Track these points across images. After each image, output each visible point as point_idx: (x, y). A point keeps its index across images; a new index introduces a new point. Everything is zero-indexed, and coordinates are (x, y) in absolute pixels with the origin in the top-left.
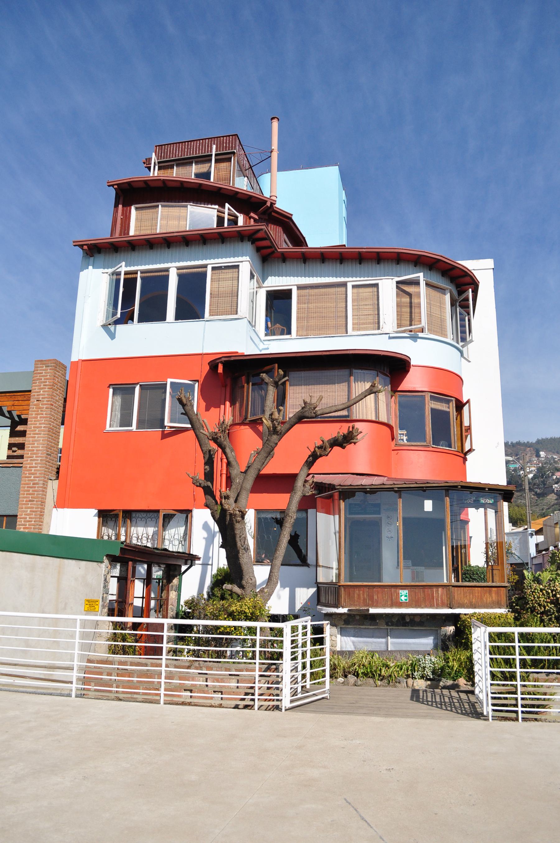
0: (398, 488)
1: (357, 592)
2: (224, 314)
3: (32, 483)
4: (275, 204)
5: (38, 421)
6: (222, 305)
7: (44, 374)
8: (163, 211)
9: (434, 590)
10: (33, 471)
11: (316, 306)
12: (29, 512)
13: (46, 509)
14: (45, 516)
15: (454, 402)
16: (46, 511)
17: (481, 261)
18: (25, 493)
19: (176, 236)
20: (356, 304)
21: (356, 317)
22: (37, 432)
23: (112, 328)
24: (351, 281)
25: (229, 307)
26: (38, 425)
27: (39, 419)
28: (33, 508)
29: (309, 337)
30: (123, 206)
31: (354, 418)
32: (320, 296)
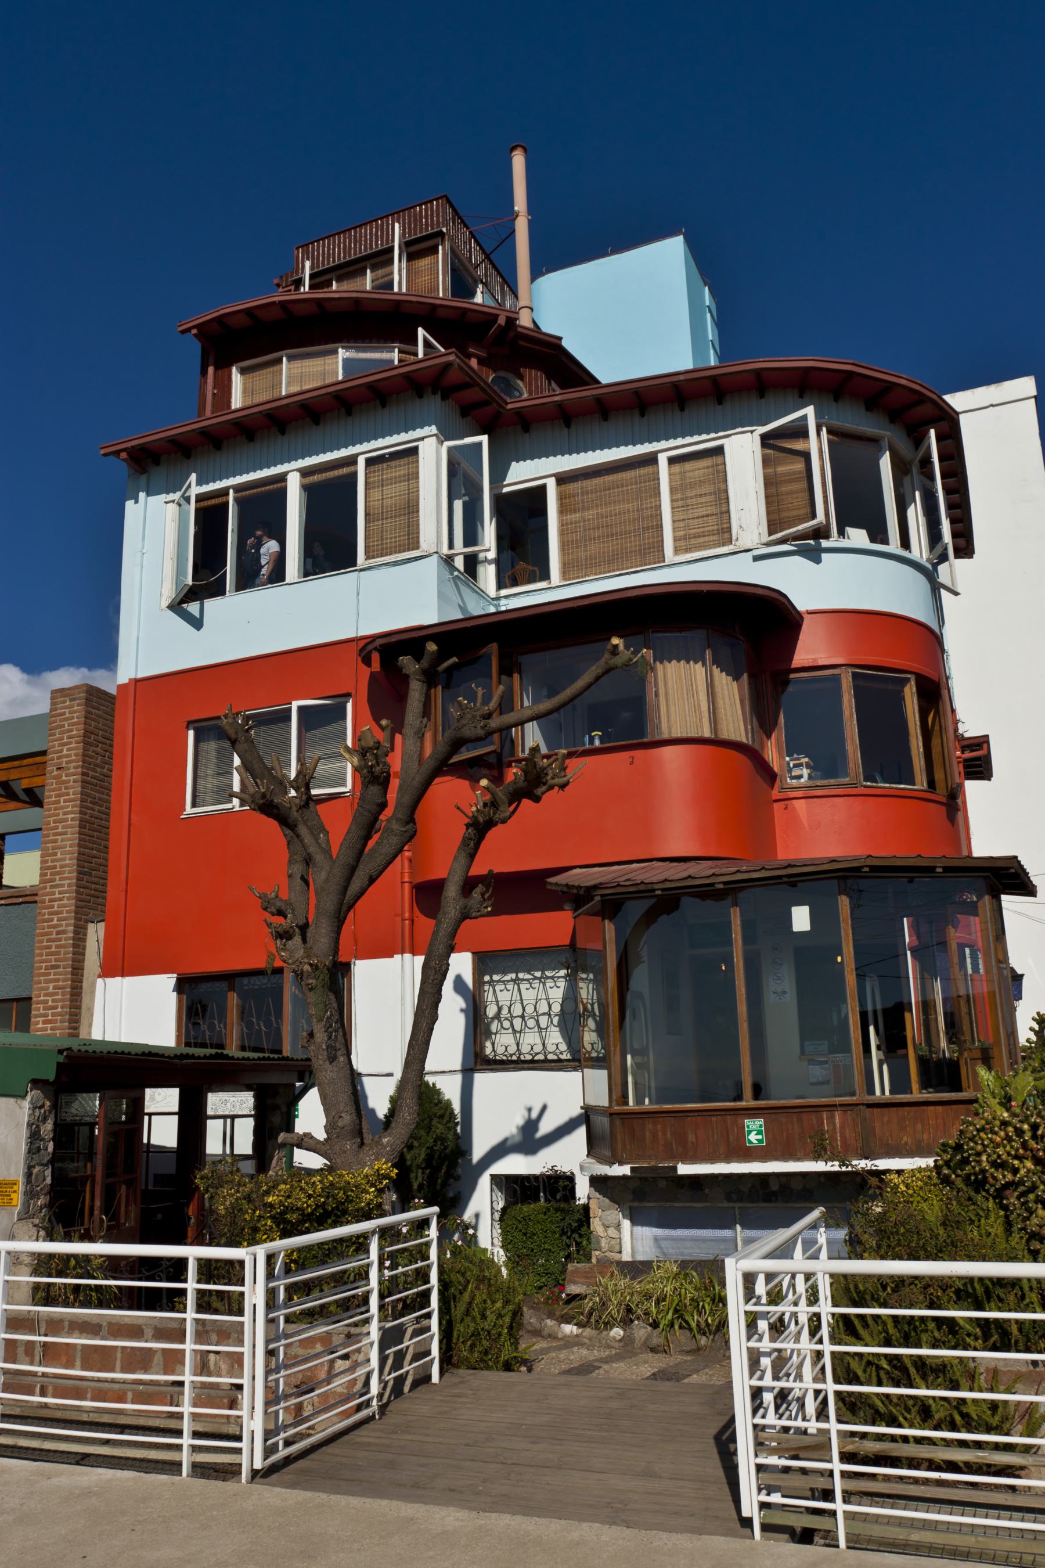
0: (725, 883)
1: (651, 1126)
2: (396, 552)
3: (54, 931)
4: (516, 319)
5: (62, 808)
6: (391, 534)
7: (67, 715)
8: (291, 366)
9: (825, 1117)
10: (56, 908)
11: (598, 514)
12: (51, 990)
13: (84, 980)
14: (83, 994)
15: (913, 683)
16: (85, 985)
17: (1007, 384)
18: (44, 952)
19: (287, 405)
20: (679, 496)
21: (682, 524)
22: (60, 830)
23: (193, 608)
24: (665, 448)
25: (404, 535)
26: (61, 816)
27: (62, 804)
28: (58, 980)
29: (587, 578)
30: (216, 369)
31: (666, 736)
32: (605, 490)
